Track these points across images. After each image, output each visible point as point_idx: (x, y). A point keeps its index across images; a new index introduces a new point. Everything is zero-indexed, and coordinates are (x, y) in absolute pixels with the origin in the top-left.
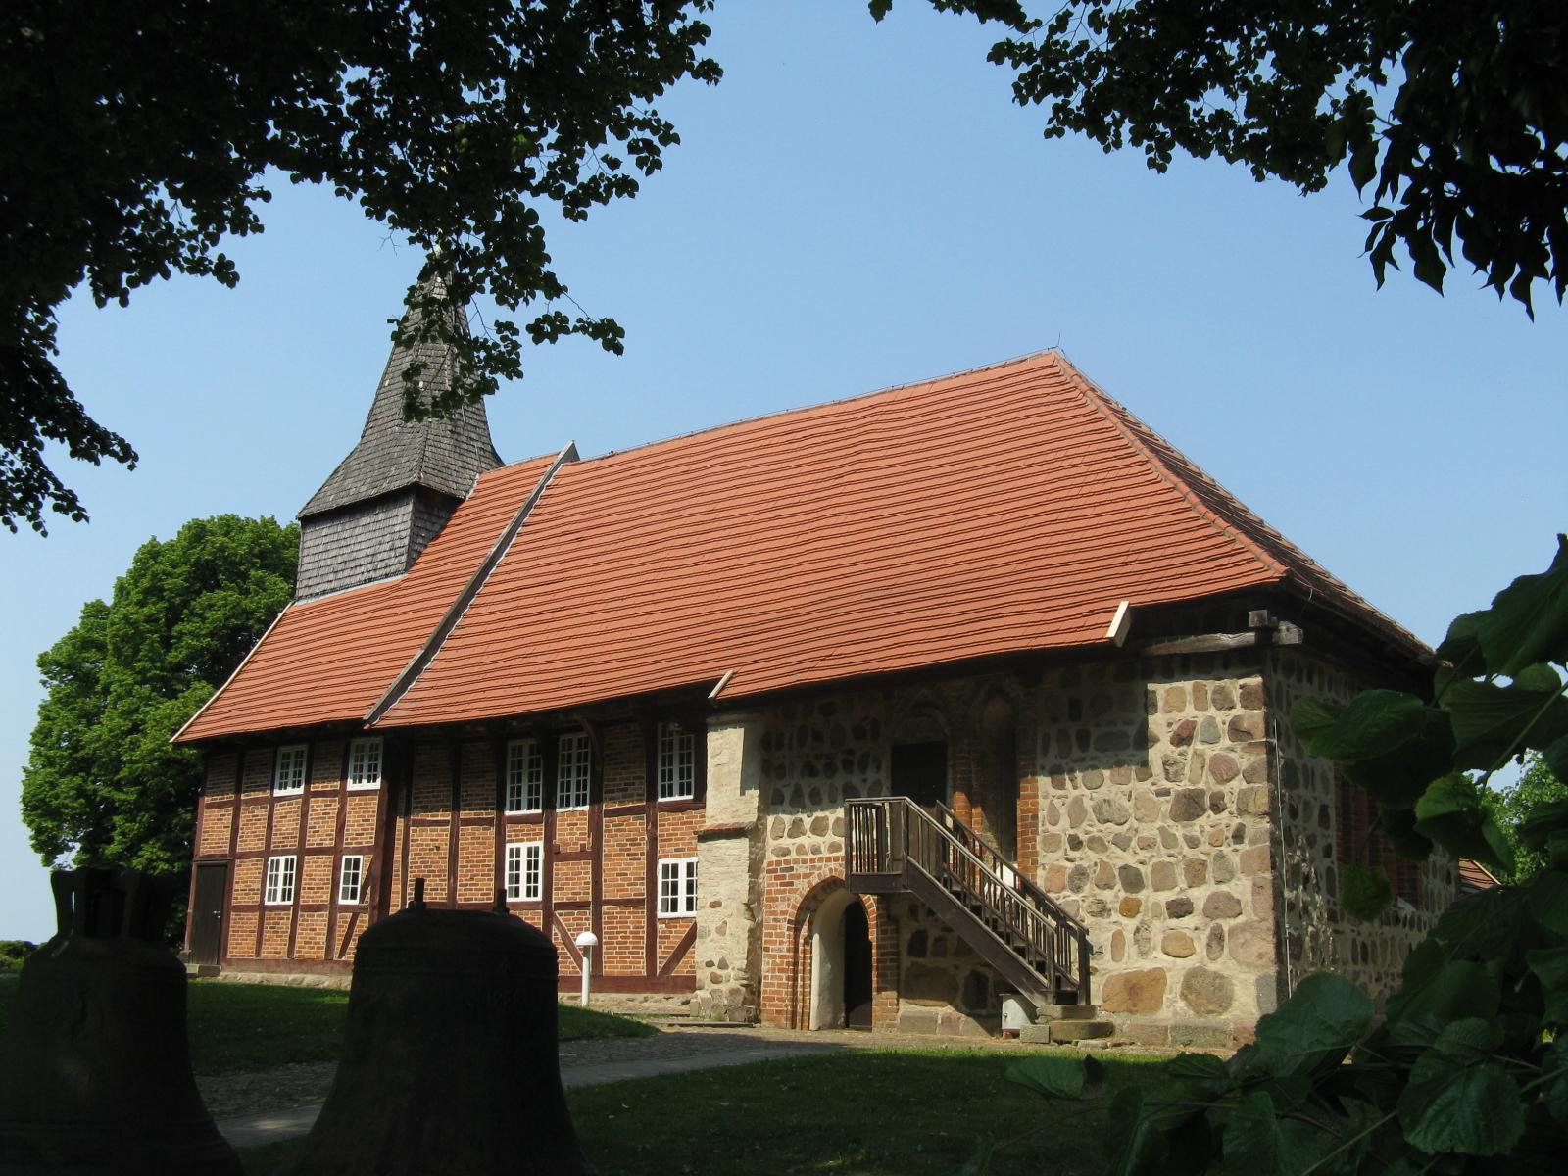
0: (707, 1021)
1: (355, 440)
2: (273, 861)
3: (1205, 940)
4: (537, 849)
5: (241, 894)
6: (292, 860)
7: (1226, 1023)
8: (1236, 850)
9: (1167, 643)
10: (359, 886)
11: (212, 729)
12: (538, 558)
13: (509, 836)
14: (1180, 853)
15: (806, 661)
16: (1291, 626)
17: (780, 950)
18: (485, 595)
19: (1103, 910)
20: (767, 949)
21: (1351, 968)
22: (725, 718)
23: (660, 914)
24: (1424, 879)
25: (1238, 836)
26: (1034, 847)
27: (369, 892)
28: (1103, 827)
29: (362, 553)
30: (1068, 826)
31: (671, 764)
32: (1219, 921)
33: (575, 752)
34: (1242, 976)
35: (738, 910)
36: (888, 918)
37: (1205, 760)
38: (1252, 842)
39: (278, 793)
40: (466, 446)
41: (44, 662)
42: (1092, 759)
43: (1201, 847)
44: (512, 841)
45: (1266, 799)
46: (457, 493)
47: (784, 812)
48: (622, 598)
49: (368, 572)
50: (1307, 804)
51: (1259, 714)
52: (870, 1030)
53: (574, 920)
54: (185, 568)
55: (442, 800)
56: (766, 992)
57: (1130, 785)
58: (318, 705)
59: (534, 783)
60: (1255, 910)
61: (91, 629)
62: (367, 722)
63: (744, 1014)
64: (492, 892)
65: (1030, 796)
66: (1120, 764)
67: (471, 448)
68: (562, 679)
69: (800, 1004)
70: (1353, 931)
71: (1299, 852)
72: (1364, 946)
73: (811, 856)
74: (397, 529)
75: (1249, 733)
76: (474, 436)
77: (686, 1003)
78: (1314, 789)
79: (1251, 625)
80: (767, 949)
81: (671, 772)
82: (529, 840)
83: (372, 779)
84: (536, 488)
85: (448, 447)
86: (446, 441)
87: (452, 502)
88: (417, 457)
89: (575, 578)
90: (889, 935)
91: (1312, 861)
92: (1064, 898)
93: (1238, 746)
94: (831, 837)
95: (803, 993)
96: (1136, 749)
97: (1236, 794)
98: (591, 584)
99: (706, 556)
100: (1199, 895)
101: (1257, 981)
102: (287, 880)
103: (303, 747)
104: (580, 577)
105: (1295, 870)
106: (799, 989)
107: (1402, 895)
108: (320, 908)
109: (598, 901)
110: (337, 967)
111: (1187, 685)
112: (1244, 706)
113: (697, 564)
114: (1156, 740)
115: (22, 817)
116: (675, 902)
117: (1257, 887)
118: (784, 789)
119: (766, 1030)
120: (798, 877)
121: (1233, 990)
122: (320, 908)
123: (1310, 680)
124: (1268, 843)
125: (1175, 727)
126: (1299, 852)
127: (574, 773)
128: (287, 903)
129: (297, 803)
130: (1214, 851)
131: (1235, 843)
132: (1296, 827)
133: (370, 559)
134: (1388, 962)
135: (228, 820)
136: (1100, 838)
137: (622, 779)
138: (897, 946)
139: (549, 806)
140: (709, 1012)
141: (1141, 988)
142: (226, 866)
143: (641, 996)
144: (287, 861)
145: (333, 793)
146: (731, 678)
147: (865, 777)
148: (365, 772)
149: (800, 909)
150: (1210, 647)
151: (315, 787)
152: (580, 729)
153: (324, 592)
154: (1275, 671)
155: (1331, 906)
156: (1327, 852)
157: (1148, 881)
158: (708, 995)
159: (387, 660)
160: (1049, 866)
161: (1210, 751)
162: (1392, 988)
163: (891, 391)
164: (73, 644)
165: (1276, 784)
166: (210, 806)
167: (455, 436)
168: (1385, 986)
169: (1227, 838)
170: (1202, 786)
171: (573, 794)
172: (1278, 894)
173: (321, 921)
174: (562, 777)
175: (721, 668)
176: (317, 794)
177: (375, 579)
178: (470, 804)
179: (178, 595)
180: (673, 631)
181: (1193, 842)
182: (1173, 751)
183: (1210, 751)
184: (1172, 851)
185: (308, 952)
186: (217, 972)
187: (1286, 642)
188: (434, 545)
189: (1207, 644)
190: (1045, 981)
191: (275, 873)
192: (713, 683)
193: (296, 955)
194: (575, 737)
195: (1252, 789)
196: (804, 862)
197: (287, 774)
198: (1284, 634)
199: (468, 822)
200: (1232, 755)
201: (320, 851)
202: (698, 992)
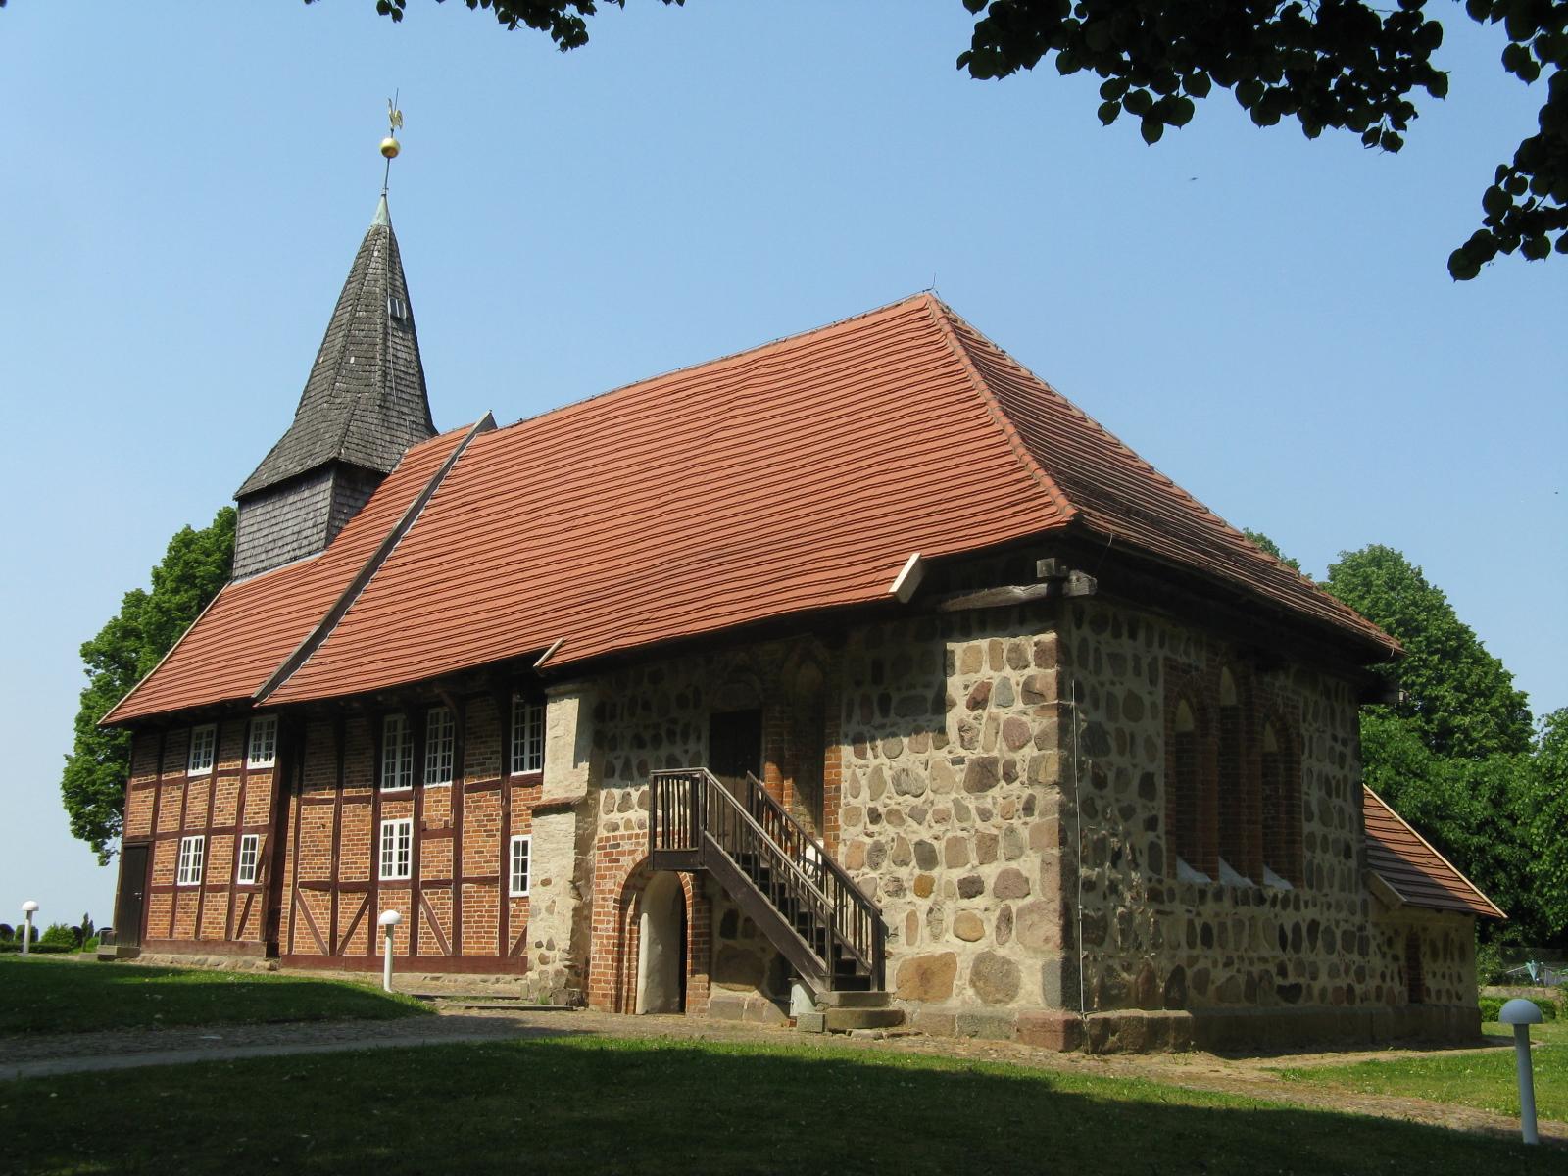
1: (288, 421)
2: (185, 842)
3: (994, 922)
4: (407, 826)
5: (158, 879)
6: (201, 840)
7: (1011, 1013)
8: (1026, 824)
9: (962, 598)
10: (255, 866)
11: (135, 710)
12: (437, 530)
13: (384, 813)
14: (973, 827)
16: (1082, 575)
17: (607, 930)
18: (387, 569)
19: (898, 890)
20: (596, 929)
22: (562, 688)
23: (512, 893)
24: (1308, 854)
25: (1028, 808)
26: (836, 820)
27: (263, 871)
28: (900, 799)
29: (289, 532)
30: (868, 799)
32: (1008, 901)
34: (1029, 962)
35: (565, 888)
37: (998, 725)
38: (1042, 815)
39: (192, 773)
40: (395, 420)
41: (89, 653)
46: (381, 468)
47: (615, 786)
48: (496, 568)
49: (294, 550)
51: (1051, 673)
53: (438, 898)
54: (217, 556)
55: (329, 778)
57: (927, 753)
60: (1043, 889)
61: (130, 618)
62: (255, 700)
63: (567, 997)
64: (369, 871)
66: (918, 731)
67: (402, 422)
69: (625, 987)
70: (1189, 912)
73: (637, 831)
74: (319, 505)
75: (1042, 695)
76: (405, 410)
78: (1133, 756)
79: (1039, 576)
80: (596, 929)
82: (401, 817)
83: (268, 757)
84: (446, 460)
85: (376, 422)
86: (374, 415)
87: (377, 477)
88: (339, 432)
89: (462, 549)
91: (1127, 834)
92: (863, 876)
93: (1031, 709)
95: (629, 975)
97: (1027, 762)
98: (474, 555)
99: (577, 523)
100: (989, 873)
101: (1043, 967)
103: (212, 727)
104: (467, 547)
106: (625, 971)
109: (459, 879)
110: (235, 948)
111: (983, 643)
112: (1038, 666)
113: (567, 530)
114: (953, 704)
115: (63, 804)
117: (1046, 864)
120: (623, 853)
121: (1019, 978)
123: (1133, 636)
124: (1057, 816)
127: (440, 748)
130: (1005, 824)
131: (1026, 815)
132: (1102, 797)
133: (295, 537)
135: (150, 801)
136: (897, 811)
137: (481, 754)
138: (710, 926)
139: (418, 783)
141: (933, 973)
142: (147, 847)
143: (493, 978)
144: (197, 841)
145: (235, 773)
146: (560, 646)
148: (263, 752)
149: (626, 887)
150: (1001, 601)
151: (223, 766)
152: (440, 703)
153: (257, 572)
154: (1079, 627)
155: (1154, 884)
156: (1151, 824)
157: (941, 857)
158: (537, 977)
160: (850, 841)
163: (774, 344)
164: (114, 634)
165: (1071, 751)
166: (137, 788)
167: (384, 410)
169: (1018, 810)
170: (995, 753)
173: (221, 901)
174: (430, 752)
177: (300, 557)
178: (351, 782)
179: (211, 582)
180: (531, 599)
181: (985, 815)
183: (1004, 715)
184: (965, 825)
186: (136, 954)
187: (1076, 593)
188: (355, 521)
189: (1000, 598)
190: (823, 964)
191: (186, 853)
192: (540, 652)
194: (442, 711)
195: (1043, 756)
196: (630, 837)
198: (1074, 583)
199: (350, 800)
200: (1024, 719)
201: (223, 831)
202: (529, 973)
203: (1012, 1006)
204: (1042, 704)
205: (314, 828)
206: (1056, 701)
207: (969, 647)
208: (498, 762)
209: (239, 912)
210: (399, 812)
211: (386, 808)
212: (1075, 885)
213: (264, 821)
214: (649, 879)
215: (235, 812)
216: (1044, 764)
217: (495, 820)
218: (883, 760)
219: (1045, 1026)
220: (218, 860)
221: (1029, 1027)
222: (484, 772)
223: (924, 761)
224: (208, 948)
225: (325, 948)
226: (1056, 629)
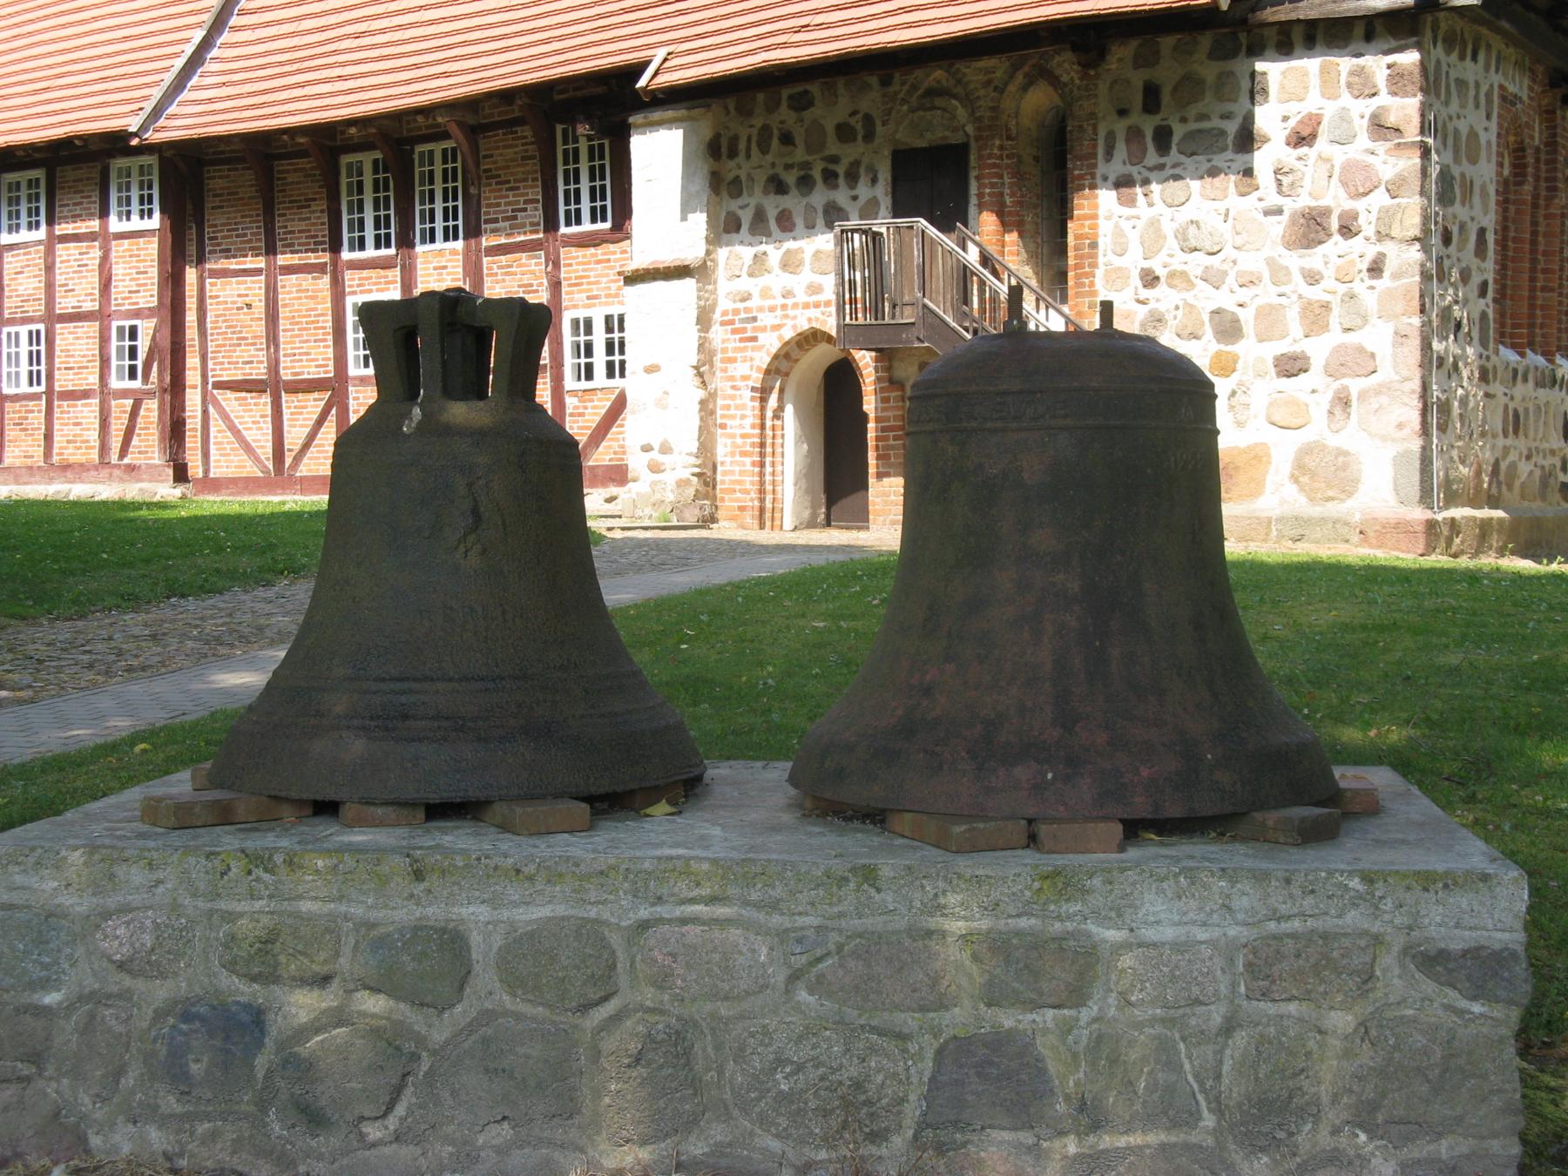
0: (647, 523)
6: (38, 332)
8: (1372, 288)
13: (350, 286)
15: (772, 34)
21: (1501, 442)
22: (657, 115)
25: (1376, 269)
26: (1092, 284)
31: (577, 181)
32: (1346, 381)
33: (438, 168)
36: (889, 381)
37: (1333, 166)
42: (1174, 166)
43: (1324, 284)
44: (354, 293)
45: (1417, 220)
47: (742, 243)
50: (1462, 227)
52: (868, 528)
55: (250, 241)
56: (723, 482)
58: (55, 113)
59: (382, 213)
62: (135, 135)
63: (697, 512)
64: (331, 363)
65: (1086, 217)
66: (1213, 172)
68: (417, 66)
69: (769, 497)
70: (1506, 394)
71: (1451, 291)
72: (1516, 415)
73: (781, 301)
75: (1397, 130)
77: (610, 500)
78: (1471, 207)
80: (723, 426)
81: (577, 192)
90: (892, 404)
91: (1466, 301)
93: (1381, 147)
94: (807, 276)
96: (1237, 152)
102: (34, 358)
103: (39, 174)
105: (1446, 313)
106: (768, 478)
107: (1559, 349)
108: (86, 394)
110: (116, 472)
114: (1266, 140)
116: (589, 369)
118: (740, 213)
119: (725, 530)
120: (764, 329)
122: (86, 394)
123: (1474, 58)
124: (1418, 278)
125: (1292, 123)
126: (1451, 291)
128: (36, 389)
129: (38, 252)
130: (1342, 288)
131: (1372, 277)
132: (1448, 257)
134: (1540, 436)
139: (406, 242)
140: (648, 511)
141: (1237, 468)
145: (91, 237)
147: (853, 193)
148: (135, 206)
149: (768, 372)
150: (1349, 10)
151: (62, 229)
152: (446, 136)
159: (151, 47)
161: (1339, 155)
162: (1543, 467)
168: (1536, 466)
169: (1360, 271)
171: (439, 225)
172: (1426, 346)
173: (88, 412)
174: (422, 203)
175: (649, 46)
176: (65, 239)
181: (1313, 278)
182: (1289, 156)
183: (1339, 155)
184: (1282, 289)
185: (74, 455)
193: (55, 459)
194: (438, 147)
195: (1399, 205)
196: (772, 309)
197: (18, 212)
199: (289, 270)
200: (1371, 159)
203: (1350, 504)
204: (1397, 141)
205: (232, 309)
206: (1419, 138)
207: (1288, 69)
208: (538, 216)
209: (118, 426)
210: (376, 284)
211: (353, 279)
212: (1431, 362)
213: (148, 302)
214: (797, 360)
215: (97, 292)
216: (1399, 216)
217: (537, 291)
218: (1160, 207)
219: (1400, 527)
220: (73, 356)
221: (1377, 528)
222: (517, 228)
223: (1223, 212)
224: (69, 474)
225: (265, 467)
226: (1419, 46)
